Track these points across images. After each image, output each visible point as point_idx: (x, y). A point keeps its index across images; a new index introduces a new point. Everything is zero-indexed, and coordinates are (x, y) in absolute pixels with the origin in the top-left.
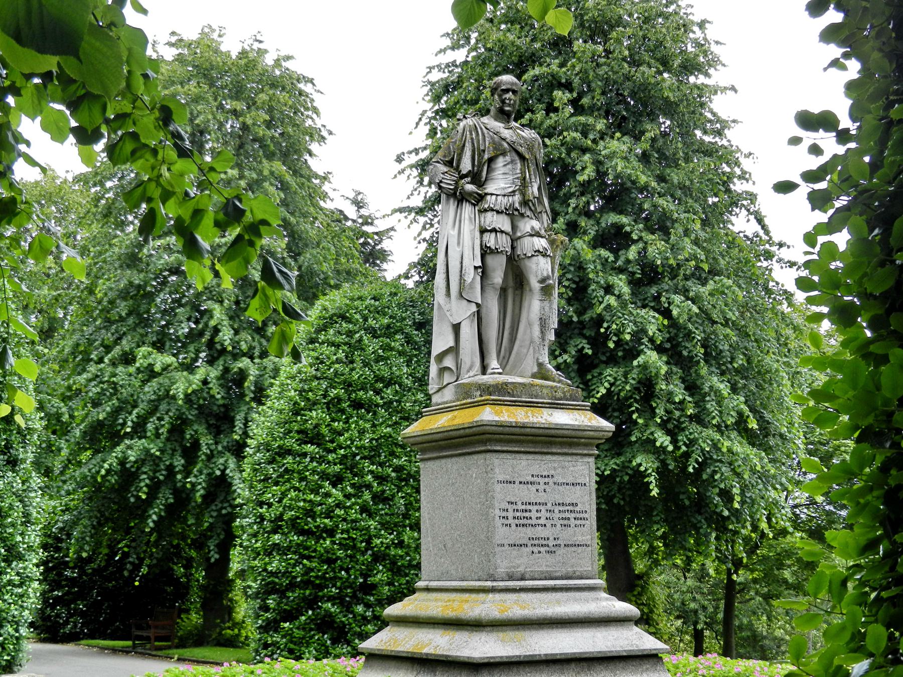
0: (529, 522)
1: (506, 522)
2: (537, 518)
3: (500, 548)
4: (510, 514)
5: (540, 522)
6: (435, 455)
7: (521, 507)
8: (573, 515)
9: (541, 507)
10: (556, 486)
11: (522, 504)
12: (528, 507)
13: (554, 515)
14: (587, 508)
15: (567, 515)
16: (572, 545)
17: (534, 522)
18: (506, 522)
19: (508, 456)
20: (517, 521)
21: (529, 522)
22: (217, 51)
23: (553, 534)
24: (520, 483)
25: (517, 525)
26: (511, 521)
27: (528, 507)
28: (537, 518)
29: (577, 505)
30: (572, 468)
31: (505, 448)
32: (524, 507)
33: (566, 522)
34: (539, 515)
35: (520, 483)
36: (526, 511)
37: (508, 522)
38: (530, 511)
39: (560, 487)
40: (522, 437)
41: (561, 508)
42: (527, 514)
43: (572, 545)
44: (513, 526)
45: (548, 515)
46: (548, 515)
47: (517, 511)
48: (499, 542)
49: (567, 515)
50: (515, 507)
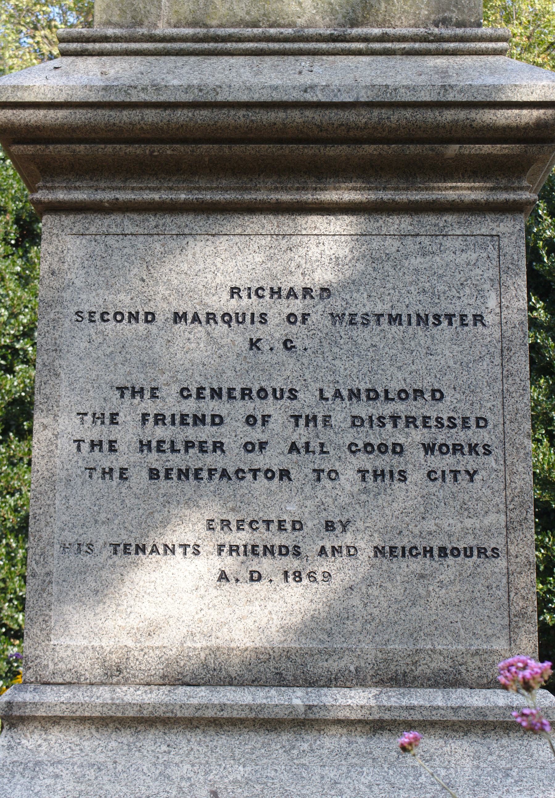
0: (212, 460)
1: (105, 460)
2: (249, 447)
3: (72, 560)
4: (127, 433)
5: (260, 461)
6: (449, 115)
7: (171, 404)
8: (418, 435)
9: (270, 406)
10: (343, 329)
11: (184, 394)
12: (210, 406)
13: (326, 435)
14: (488, 404)
15: (390, 435)
16: (411, 552)
17: (232, 459)
18: (105, 460)
19: (127, 223)
20: (153, 459)
21: (212, 460)
22: (245, 203)
23: (322, 507)
24: (178, 317)
25: (153, 474)
26: (128, 455)
27: (210, 406)
28: (249, 447)
29: (437, 395)
30: (416, 261)
31: (124, 196)
32: (190, 406)
33: (384, 462)
34: (256, 434)
35: (178, 317)
36: (199, 420)
37: (116, 462)
38: (217, 420)
39: (361, 334)
40: (168, 150)
41: (363, 409)
42: (205, 433)
43: (411, 552)
44: (139, 478)
45: (301, 435)
46: (301, 435)
47: (159, 419)
48: (70, 537)
49: (390, 435)
50: (149, 406)
